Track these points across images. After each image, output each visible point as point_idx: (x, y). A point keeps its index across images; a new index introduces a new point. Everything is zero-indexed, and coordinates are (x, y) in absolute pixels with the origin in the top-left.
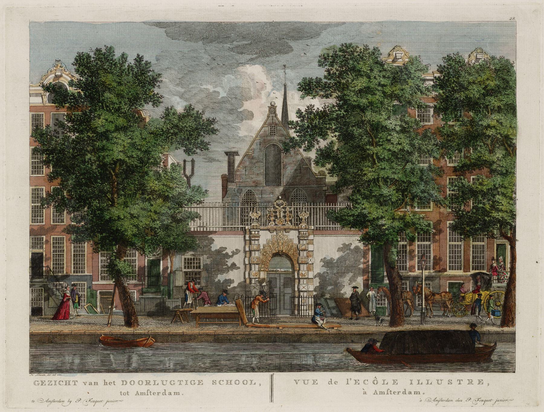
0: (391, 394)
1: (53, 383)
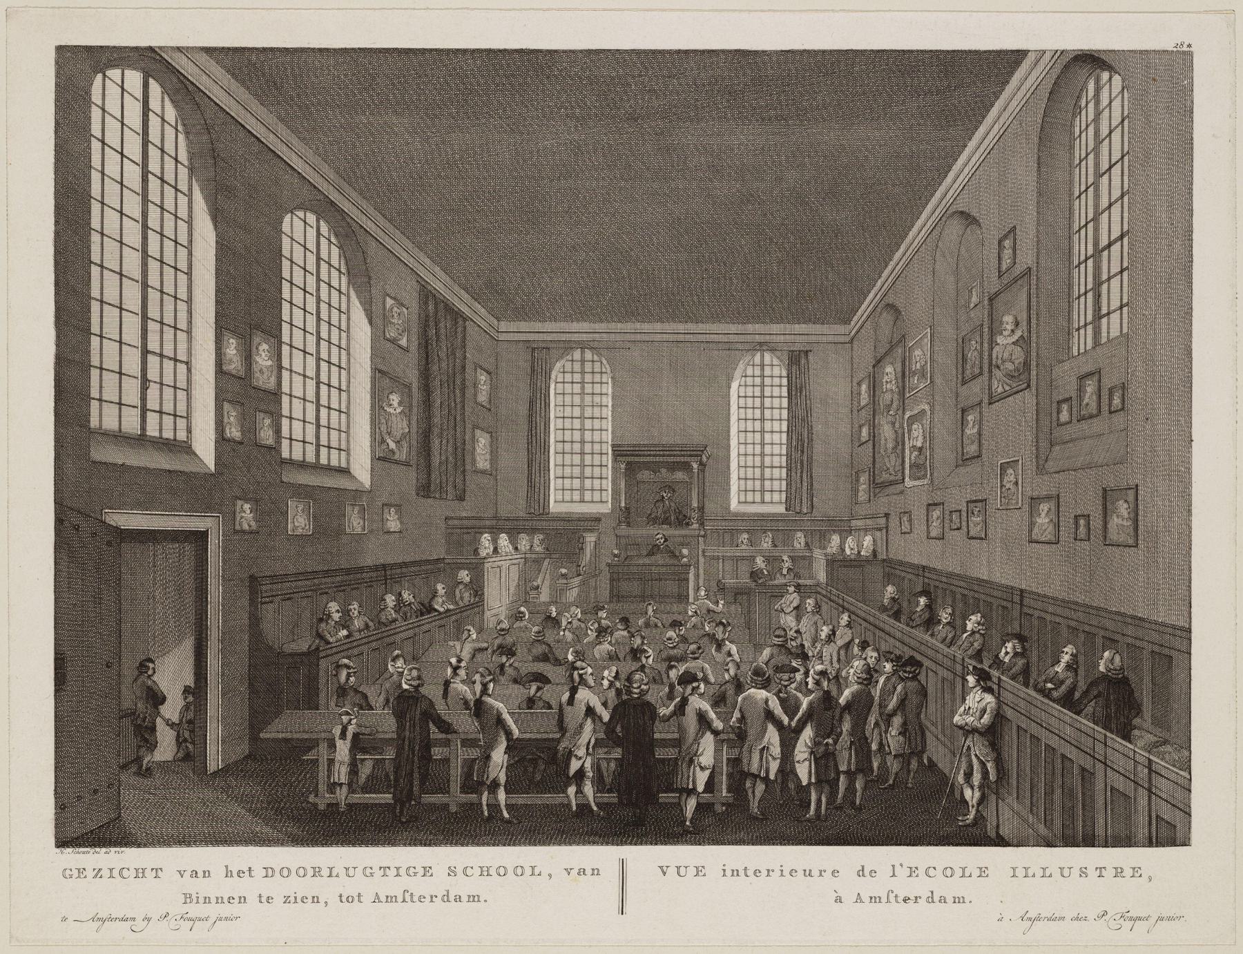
0: (897, 902)
1: (106, 873)
